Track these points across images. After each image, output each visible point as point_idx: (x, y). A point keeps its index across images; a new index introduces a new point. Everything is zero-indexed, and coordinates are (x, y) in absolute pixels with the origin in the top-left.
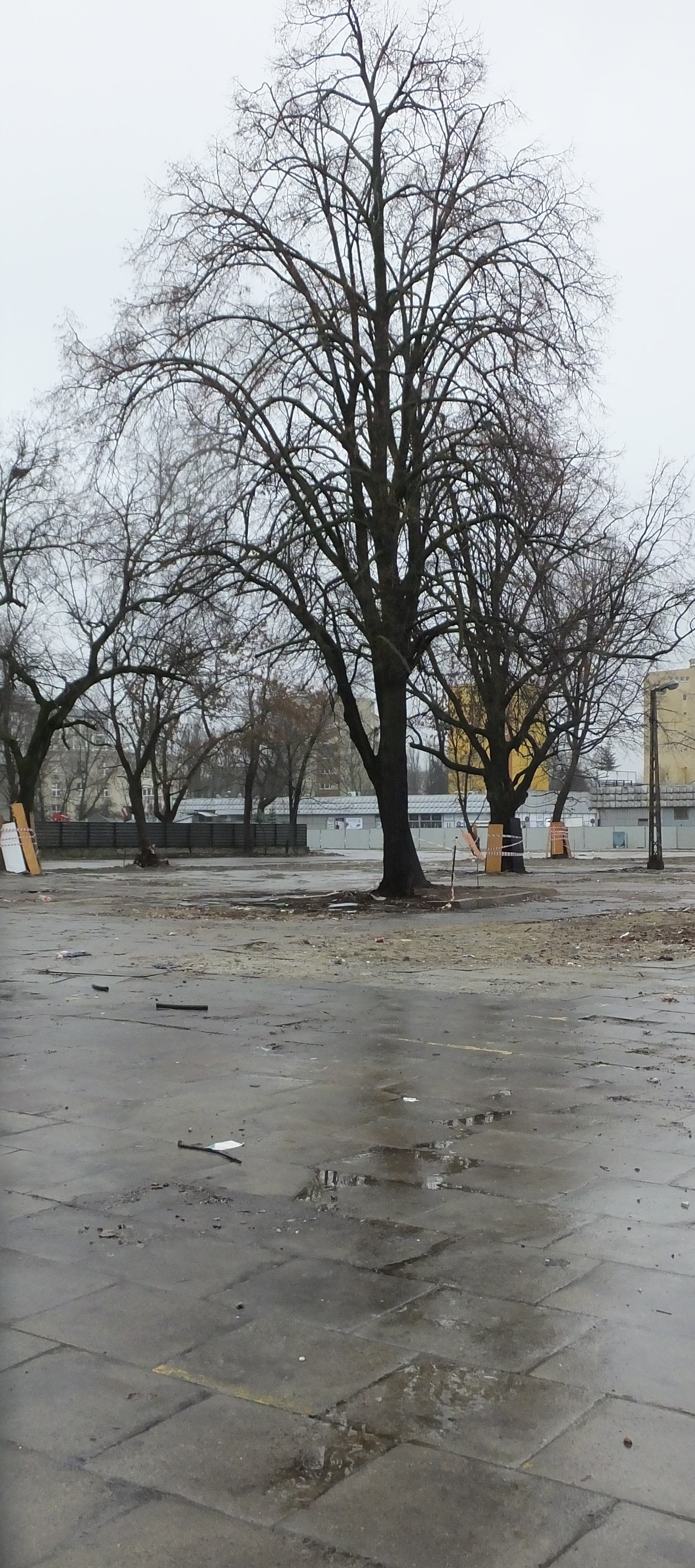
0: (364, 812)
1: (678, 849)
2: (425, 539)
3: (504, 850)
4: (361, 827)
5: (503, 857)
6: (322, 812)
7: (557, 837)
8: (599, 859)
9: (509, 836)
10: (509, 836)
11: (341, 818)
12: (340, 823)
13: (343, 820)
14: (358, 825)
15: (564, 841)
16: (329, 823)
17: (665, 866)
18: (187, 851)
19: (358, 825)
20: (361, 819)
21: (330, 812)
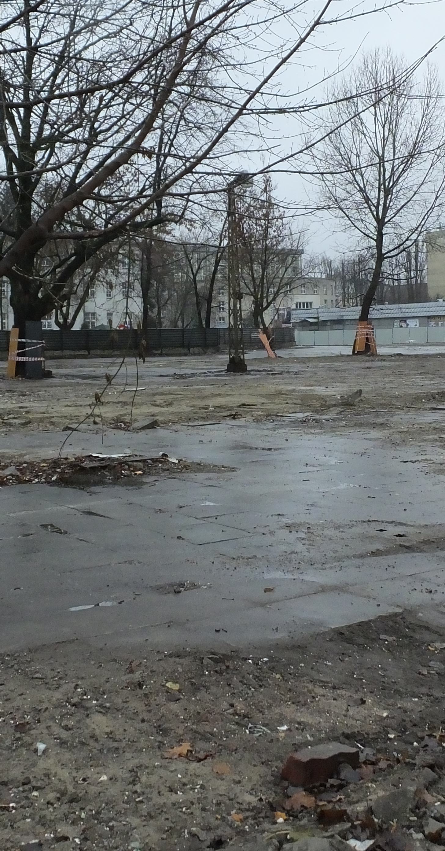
0: (419, 315)
1: (428, 344)
2: (10, 148)
3: (19, 355)
4: (418, 326)
5: (18, 362)
6: (390, 316)
7: (361, 335)
8: (401, 355)
9: (24, 340)
10: (24, 340)
11: (404, 319)
12: (403, 324)
13: (405, 322)
14: (416, 325)
15: (367, 339)
16: (395, 324)
17: (249, 368)
18: (186, 351)
19: (416, 325)
20: (418, 320)
21: (395, 315)
